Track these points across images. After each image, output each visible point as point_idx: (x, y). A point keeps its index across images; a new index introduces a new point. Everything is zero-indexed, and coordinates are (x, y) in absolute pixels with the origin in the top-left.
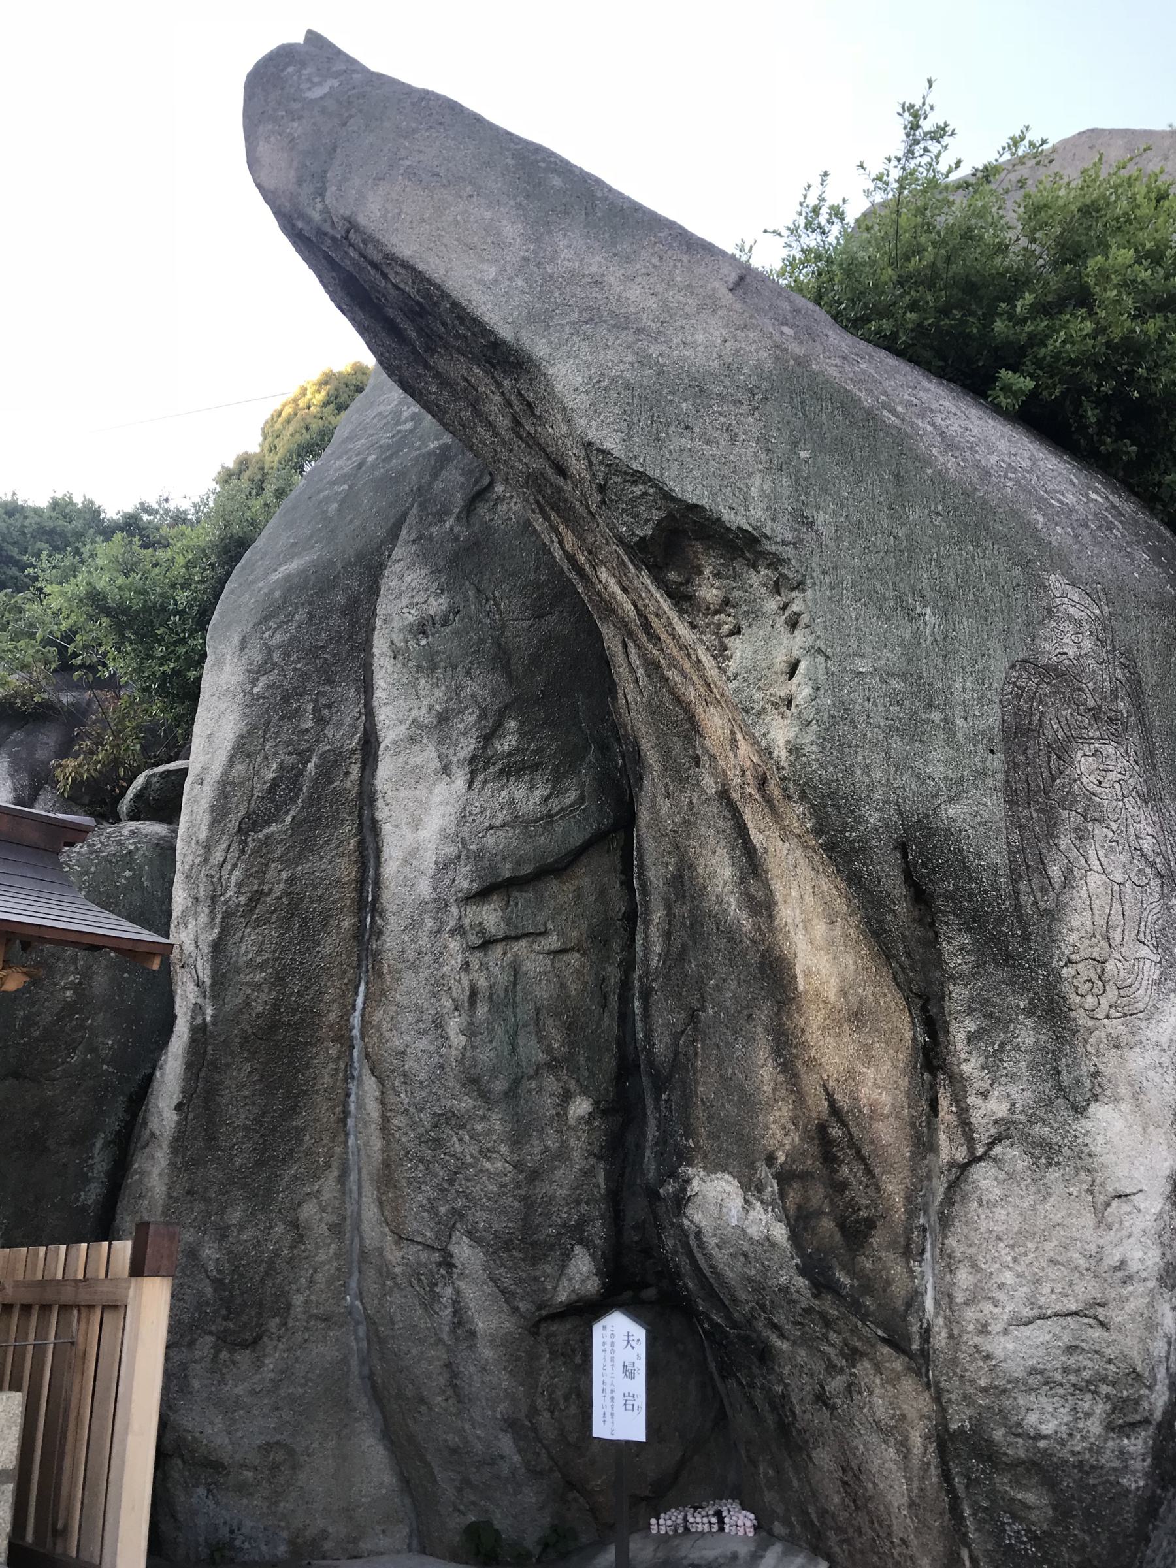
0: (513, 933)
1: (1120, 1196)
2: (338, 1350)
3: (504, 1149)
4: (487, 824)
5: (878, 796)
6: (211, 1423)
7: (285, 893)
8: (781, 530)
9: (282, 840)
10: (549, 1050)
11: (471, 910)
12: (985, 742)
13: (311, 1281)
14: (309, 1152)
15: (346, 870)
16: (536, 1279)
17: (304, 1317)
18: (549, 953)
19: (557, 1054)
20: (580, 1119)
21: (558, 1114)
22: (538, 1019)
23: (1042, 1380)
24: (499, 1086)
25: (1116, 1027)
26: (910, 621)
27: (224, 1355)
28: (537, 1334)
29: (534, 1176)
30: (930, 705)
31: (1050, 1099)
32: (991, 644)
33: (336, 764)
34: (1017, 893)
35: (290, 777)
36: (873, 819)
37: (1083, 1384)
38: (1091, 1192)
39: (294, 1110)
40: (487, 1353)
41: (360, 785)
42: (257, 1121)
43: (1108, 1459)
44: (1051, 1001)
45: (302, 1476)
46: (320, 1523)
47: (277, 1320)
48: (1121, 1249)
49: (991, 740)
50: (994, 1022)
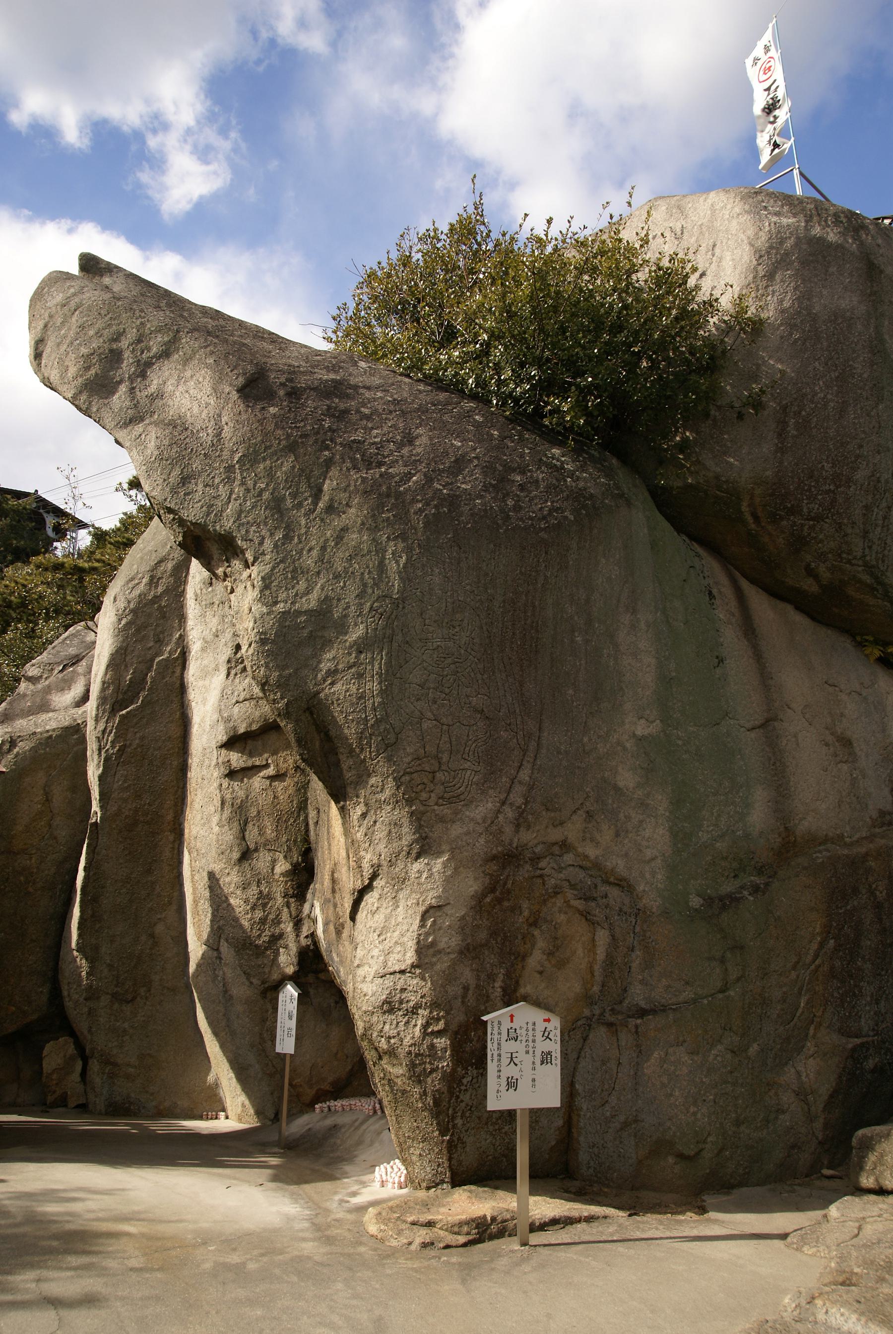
3: (238, 892)
4: (234, 701)
16: (259, 966)
18: (268, 778)
25: (446, 811)
27: (116, 1006)
28: (265, 997)
33: (167, 667)
39: (149, 871)
40: (239, 1008)
47: (145, 989)
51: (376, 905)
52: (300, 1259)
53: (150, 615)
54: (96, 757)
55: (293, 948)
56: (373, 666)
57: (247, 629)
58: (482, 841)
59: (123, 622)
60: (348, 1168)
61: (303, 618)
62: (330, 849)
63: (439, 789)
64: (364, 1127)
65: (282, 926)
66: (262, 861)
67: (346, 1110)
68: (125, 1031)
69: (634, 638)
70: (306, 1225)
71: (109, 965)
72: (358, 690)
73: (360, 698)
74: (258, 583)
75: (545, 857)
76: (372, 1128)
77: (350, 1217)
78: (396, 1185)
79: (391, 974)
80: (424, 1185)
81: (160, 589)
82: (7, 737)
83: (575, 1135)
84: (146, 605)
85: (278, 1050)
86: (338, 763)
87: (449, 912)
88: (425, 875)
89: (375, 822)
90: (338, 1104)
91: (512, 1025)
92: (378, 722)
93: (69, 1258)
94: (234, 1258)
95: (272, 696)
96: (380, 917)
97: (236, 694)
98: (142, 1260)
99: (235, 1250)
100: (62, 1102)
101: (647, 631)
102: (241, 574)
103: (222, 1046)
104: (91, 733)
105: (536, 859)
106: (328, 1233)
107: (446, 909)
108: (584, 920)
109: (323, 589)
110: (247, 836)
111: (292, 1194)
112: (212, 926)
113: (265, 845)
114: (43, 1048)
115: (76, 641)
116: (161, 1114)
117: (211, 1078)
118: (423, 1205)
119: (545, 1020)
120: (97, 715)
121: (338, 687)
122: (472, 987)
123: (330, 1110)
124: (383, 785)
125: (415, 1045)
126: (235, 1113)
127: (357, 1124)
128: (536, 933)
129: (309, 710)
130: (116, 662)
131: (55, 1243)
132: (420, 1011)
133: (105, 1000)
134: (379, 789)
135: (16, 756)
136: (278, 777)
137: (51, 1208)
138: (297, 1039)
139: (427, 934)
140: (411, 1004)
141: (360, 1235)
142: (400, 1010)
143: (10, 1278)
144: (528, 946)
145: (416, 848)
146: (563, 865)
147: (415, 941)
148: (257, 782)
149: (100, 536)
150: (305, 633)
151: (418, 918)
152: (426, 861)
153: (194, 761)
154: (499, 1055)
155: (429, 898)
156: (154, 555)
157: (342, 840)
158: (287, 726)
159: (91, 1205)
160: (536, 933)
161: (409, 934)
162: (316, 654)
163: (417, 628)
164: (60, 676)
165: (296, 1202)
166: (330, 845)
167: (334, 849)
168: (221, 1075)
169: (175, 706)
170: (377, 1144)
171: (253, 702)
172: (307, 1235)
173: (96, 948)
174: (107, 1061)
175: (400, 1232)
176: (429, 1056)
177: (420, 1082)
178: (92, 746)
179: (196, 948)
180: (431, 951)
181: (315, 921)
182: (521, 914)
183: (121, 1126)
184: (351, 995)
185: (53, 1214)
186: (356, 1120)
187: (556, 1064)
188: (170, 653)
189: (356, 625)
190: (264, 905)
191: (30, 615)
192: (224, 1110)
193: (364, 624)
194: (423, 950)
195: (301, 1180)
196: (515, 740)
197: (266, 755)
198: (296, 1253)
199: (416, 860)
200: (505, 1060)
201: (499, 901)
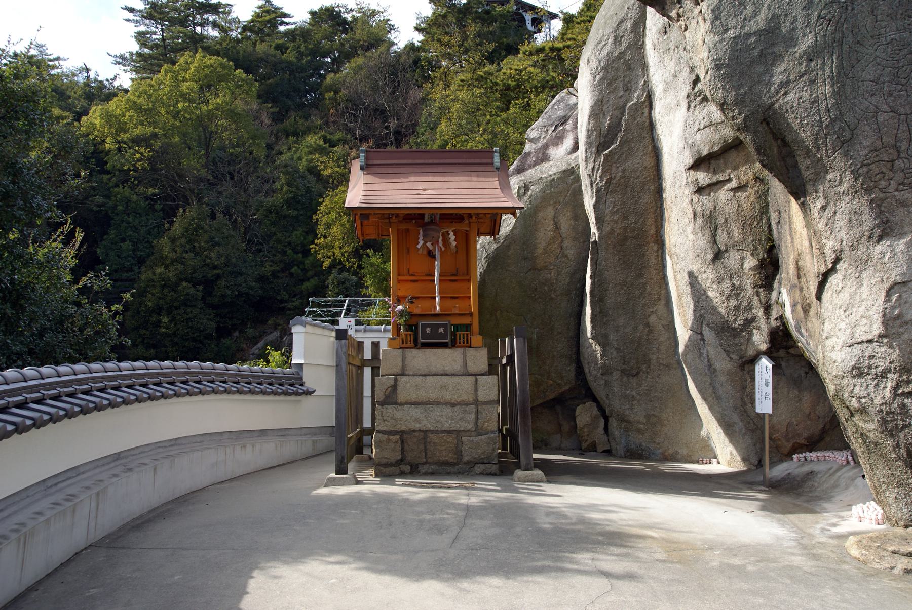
3: (715, 286)
16: (737, 344)
18: (732, 190)
39: (640, 276)
40: (722, 378)
51: (840, 285)
52: (791, 568)
53: (618, 69)
54: (589, 190)
55: (765, 329)
56: (824, 71)
57: (702, 59)
59: (597, 79)
60: (826, 505)
61: (753, 39)
62: (793, 242)
63: (899, 176)
64: (839, 474)
65: (754, 311)
66: (732, 259)
67: (821, 461)
68: (633, 397)
70: (794, 544)
71: (616, 349)
72: (810, 95)
73: (813, 103)
74: (709, 16)
76: (847, 475)
77: (834, 542)
78: (874, 521)
79: (859, 343)
80: (902, 523)
81: (623, 46)
82: (522, 184)
84: (613, 62)
85: (758, 410)
86: (796, 165)
88: (888, 256)
89: (835, 213)
90: (814, 455)
92: (832, 121)
93: (612, 548)
94: (736, 561)
95: (730, 114)
96: (845, 296)
97: (697, 123)
98: (665, 555)
99: (736, 555)
100: (592, 449)
102: (692, 11)
103: (711, 408)
104: (584, 174)
106: (814, 551)
109: (769, 9)
110: (718, 240)
111: (779, 521)
112: (695, 315)
113: (734, 246)
114: (575, 410)
115: (562, 106)
116: (666, 459)
117: (703, 433)
118: (902, 539)
120: (586, 157)
121: (791, 96)
123: (806, 459)
124: (841, 179)
125: (886, 404)
126: (726, 458)
127: (831, 471)
129: (766, 121)
130: (596, 113)
131: (601, 538)
132: (889, 375)
133: (616, 375)
134: (837, 183)
135: (530, 197)
136: (741, 188)
137: (595, 516)
138: (773, 402)
139: (893, 308)
140: (880, 369)
141: (843, 556)
142: (869, 374)
143: (574, 556)
145: (877, 232)
147: (881, 315)
148: (723, 195)
149: (569, 20)
150: (756, 53)
151: (883, 294)
152: (888, 243)
153: (667, 184)
155: (893, 275)
156: (615, 18)
157: (804, 232)
158: (747, 139)
159: (623, 516)
161: (874, 308)
162: (768, 69)
163: (868, 26)
164: (554, 134)
165: (783, 526)
166: (792, 239)
167: (797, 242)
168: (711, 431)
169: (647, 141)
170: (852, 488)
171: (713, 128)
172: (795, 551)
173: (606, 336)
174: (623, 419)
175: (881, 558)
176: (901, 414)
177: (892, 436)
178: (585, 182)
179: (683, 334)
180: (898, 322)
181: (783, 306)
183: (637, 466)
184: (821, 362)
185: (596, 520)
186: (831, 469)
188: (638, 98)
189: (804, 35)
190: (737, 295)
191: (525, 93)
192: (716, 457)
193: (813, 33)
194: (890, 322)
195: (785, 511)
197: (728, 171)
198: (787, 563)
199: (878, 243)
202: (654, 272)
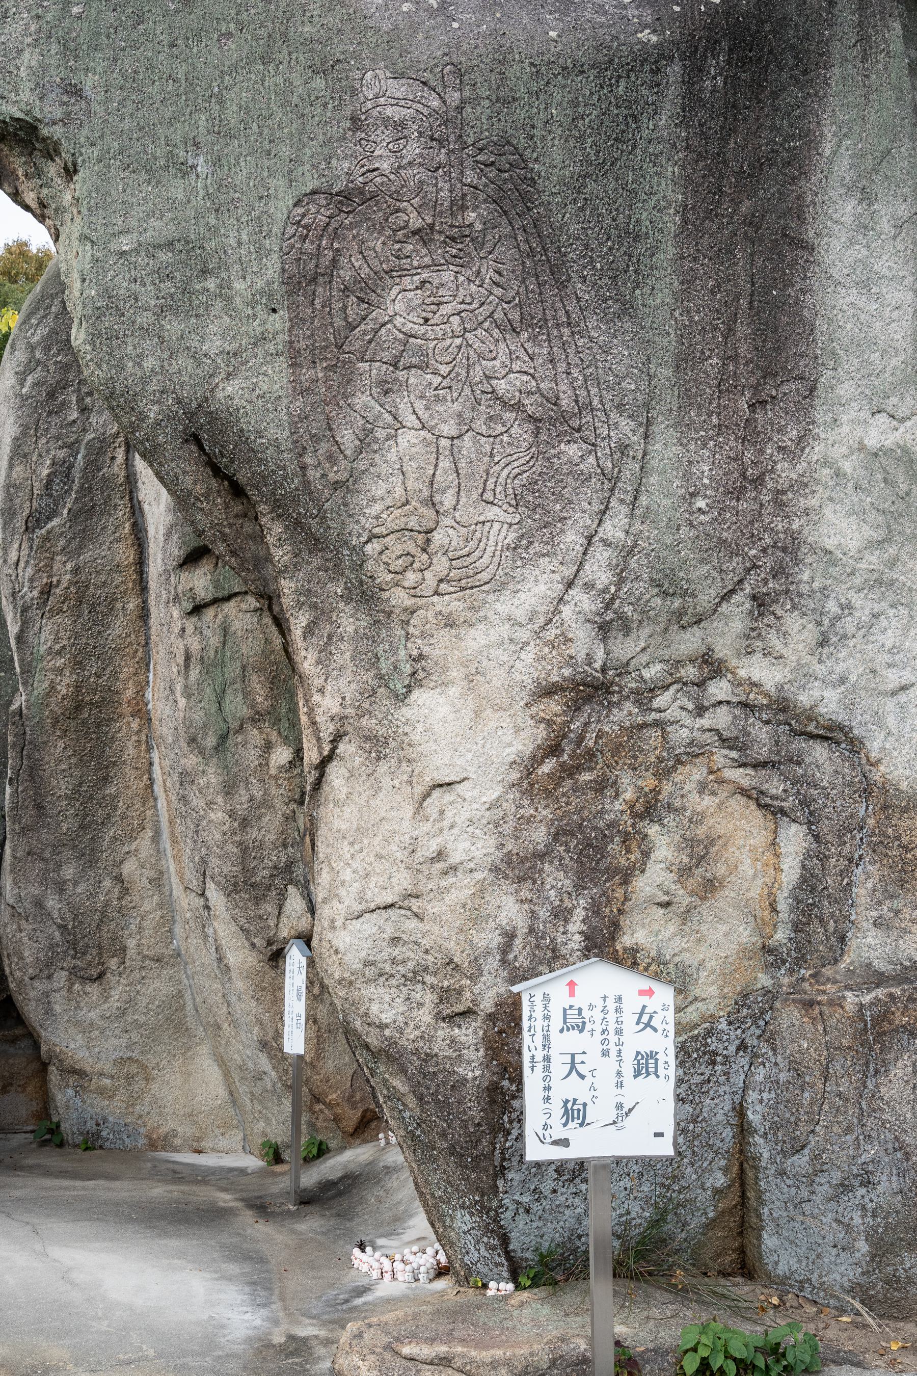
0: (220, 595)
1: (441, 786)
2: (173, 986)
5: (153, 387)
6: (73, 1039)
7: (71, 582)
8: (49, 110)
9: (62, 533)
10: (253, 705)
11: (184, 576)
12: (264, 301)
13: (140, 928)
14: (124, 817)
15: (125, 554)
16: (261, 917)
17: (139, 958)
19: (260, 708)
20: (280, 768)
21: (260, 765)
22: (244, 676)
23: (377, 972)
24: (210, 741)
25: (452, 604)
26: (183, 177)
27: (77, 987)
29: (245, 823)
30: (204, 272)
31: (373, 689)
32: (272, 182)
33: (101, 451)
34: (303, 468)
35: (62, 470)
36: (153, 413)
37: (411, 975)
38: (410, 783)
39: (106, 780)
40: (240, 984)
41: (127, 468)
42: (75, 791)
43: (440, 1047)
44: (361, 583)
45: (154, 1087)
46: (171, 1124)
47: (116, 959)
48: (438, 840)
49: (270, 296)
50: (321, 614)
58: (528, 656)
69: (864, 252)
75: (666, 687)
83: (753, 1203)
87: (468, 795)
91: (572, 1001)
101: (895, 238)
105: (645, 695)
107: (459, 788)
108: (753, 806)
119: (642, 993)
122: (521, 932)
128: (653, 830)
140: (411, 965)
144: (636, 855)
146: (706, 704)
154: (547, 1059)
160: (653, 830)
169: (122, 513)
182: (617, 795)
187: (667, 1077)
196: (591, 460)
200: (559, 1068)
201: (570, 771)
202: (131, 773)
